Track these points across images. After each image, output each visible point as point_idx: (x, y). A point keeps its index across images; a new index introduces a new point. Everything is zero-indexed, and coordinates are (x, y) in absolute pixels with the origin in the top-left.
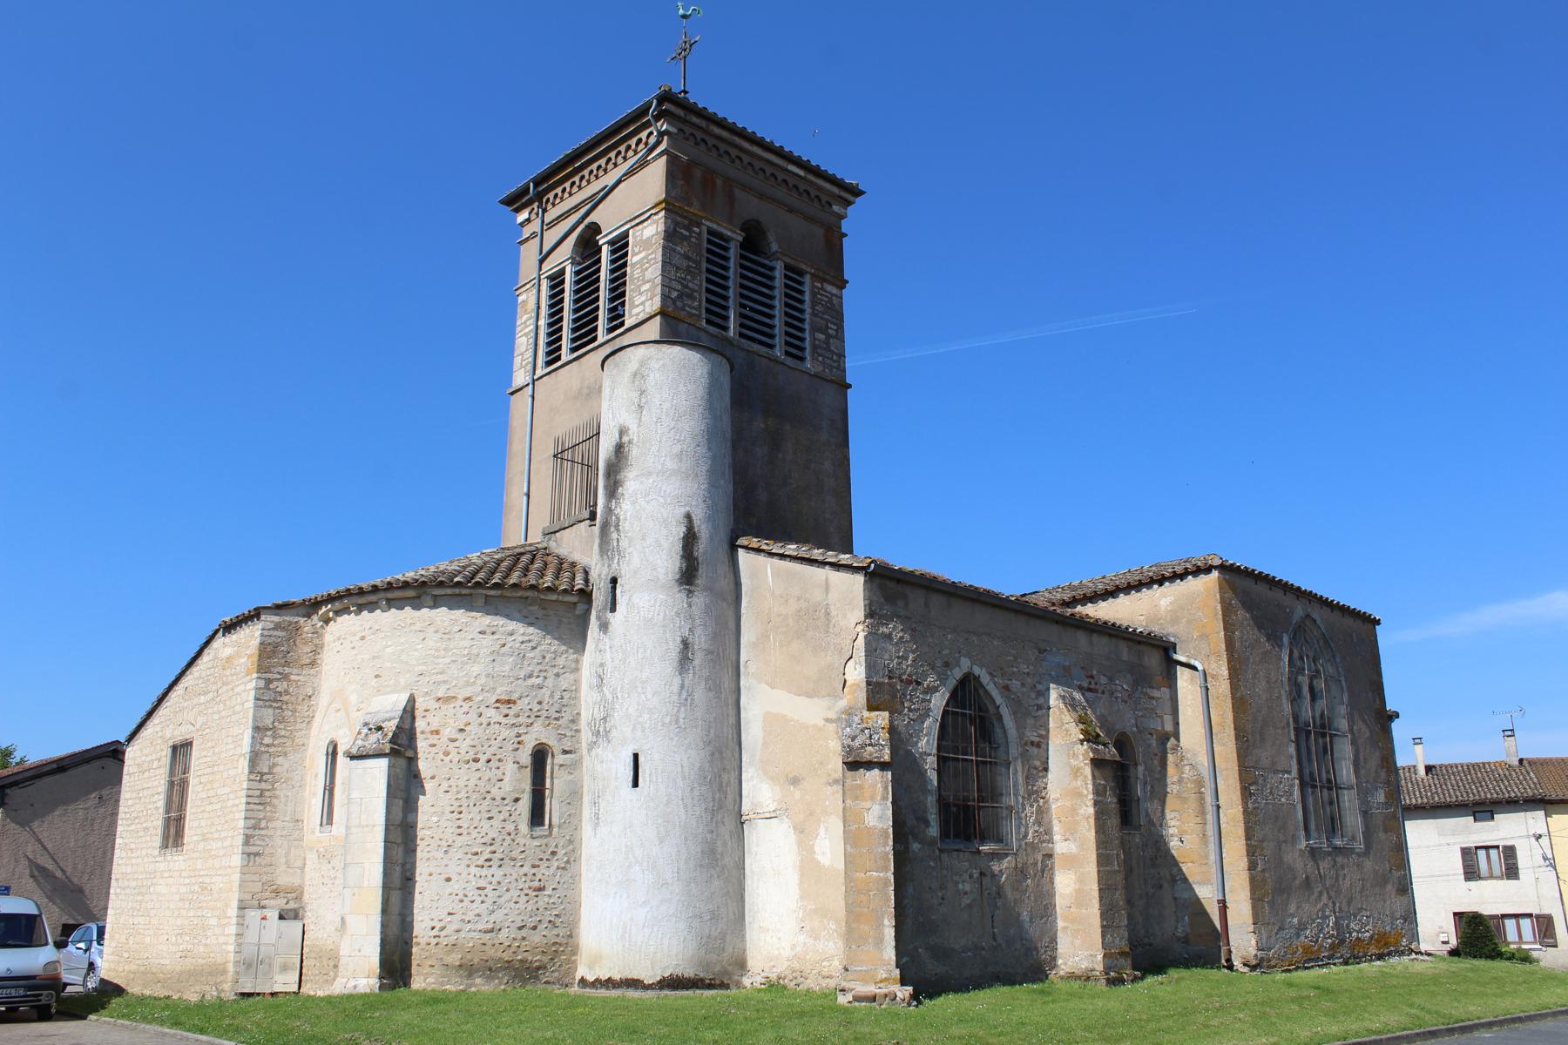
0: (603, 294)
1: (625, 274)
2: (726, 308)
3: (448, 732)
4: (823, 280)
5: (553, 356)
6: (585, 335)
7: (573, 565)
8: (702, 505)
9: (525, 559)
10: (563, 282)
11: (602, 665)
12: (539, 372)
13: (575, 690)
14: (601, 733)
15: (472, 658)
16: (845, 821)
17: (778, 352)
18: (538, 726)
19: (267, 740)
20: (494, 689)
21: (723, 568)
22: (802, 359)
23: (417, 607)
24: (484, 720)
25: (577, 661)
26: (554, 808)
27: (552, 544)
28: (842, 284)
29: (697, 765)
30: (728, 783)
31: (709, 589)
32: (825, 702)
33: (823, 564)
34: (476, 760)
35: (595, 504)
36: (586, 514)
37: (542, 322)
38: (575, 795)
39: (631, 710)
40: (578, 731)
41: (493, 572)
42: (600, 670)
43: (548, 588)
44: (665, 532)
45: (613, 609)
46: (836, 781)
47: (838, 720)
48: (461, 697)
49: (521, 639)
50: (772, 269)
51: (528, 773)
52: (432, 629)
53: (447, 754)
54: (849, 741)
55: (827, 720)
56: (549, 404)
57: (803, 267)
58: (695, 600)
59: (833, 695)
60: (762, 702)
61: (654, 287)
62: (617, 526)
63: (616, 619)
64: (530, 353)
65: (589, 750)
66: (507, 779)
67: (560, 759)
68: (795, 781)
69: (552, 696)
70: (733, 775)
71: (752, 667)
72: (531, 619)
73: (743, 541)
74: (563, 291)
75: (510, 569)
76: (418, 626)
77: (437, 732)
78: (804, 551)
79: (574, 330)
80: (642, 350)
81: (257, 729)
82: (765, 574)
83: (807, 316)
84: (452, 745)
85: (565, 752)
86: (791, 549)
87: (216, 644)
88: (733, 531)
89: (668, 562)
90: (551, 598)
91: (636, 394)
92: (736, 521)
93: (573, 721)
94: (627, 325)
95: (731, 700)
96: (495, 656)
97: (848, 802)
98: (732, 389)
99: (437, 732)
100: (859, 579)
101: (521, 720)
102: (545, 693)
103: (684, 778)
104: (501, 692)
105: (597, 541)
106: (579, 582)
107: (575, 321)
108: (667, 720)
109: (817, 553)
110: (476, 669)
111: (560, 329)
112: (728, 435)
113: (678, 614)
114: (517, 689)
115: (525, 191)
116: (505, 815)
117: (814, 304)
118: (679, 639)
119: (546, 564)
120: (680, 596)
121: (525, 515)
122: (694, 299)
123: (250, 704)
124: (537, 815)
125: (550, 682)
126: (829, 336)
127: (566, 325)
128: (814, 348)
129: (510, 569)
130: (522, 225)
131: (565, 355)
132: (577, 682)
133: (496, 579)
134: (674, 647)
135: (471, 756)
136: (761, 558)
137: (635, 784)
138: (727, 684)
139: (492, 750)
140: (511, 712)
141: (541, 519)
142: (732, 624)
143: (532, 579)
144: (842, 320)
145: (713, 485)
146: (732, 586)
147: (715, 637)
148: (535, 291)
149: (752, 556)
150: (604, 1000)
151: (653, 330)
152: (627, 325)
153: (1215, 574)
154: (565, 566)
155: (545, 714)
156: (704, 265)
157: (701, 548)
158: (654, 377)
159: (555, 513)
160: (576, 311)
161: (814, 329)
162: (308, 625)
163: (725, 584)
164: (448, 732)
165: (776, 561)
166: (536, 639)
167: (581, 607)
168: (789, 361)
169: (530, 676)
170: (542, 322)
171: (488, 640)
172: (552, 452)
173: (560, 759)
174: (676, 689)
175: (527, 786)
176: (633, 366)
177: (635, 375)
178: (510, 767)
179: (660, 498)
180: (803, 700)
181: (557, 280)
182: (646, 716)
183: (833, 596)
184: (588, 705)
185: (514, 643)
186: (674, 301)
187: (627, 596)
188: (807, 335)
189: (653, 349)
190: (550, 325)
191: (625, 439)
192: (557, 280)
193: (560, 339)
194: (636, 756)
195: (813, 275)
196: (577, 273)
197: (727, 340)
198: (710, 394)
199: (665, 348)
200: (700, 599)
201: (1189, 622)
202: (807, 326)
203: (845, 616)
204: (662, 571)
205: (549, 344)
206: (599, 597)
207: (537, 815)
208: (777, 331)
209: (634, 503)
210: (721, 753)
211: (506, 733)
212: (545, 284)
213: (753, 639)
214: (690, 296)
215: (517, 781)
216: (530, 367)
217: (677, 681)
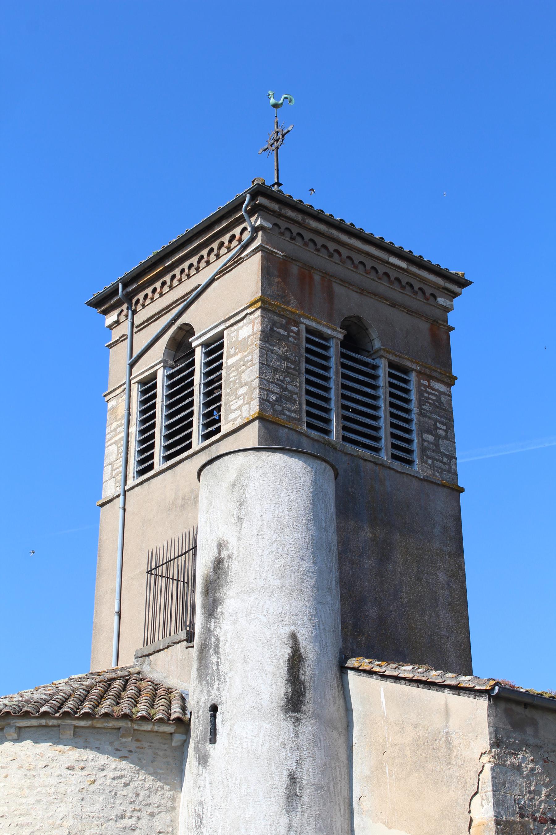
5: (145, 465)
45: (213, 740)
52: (15, 765)
61: (252, 390)
62: (217, 648)
91: (234, 506)
94: (224, 430)
100: (483, 703)
110: (63, 809)
115: (115, 292)
165: (389, 684)
183: (454, 723)
191: (224, 554)
209: (234, 622)
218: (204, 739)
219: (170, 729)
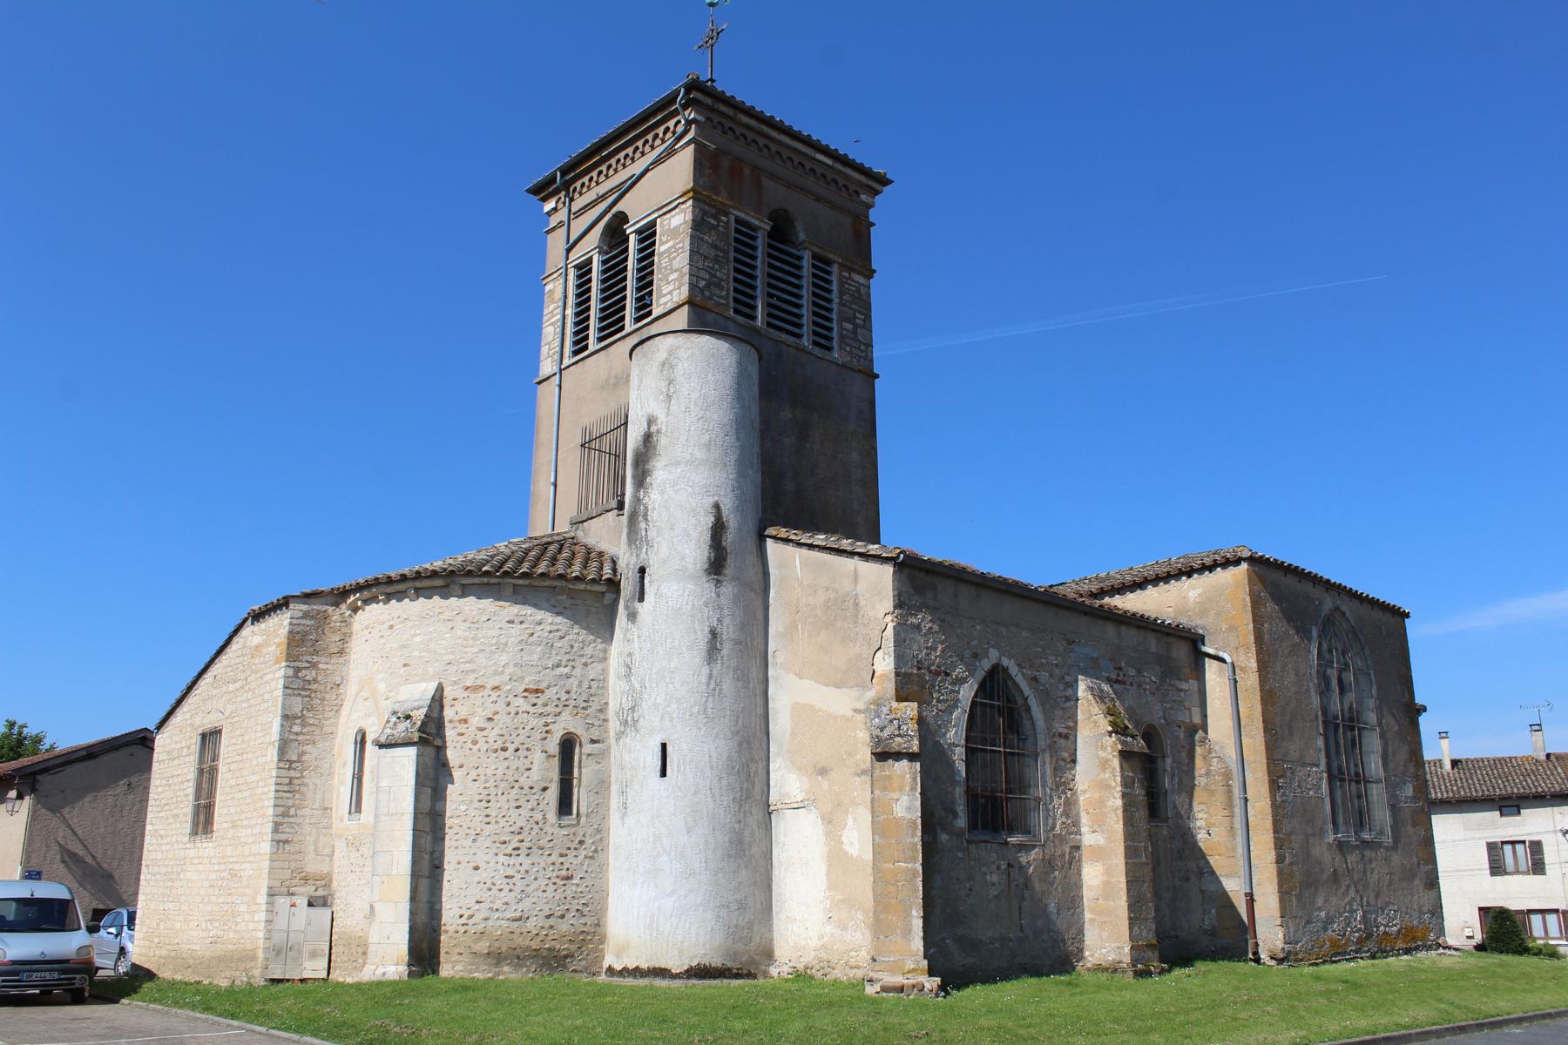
1: (652, 264)
2: (754, 298)
3: (476, 721)
4: (850, 270)
5: (580, 345)
6: (612, 325)
7: (601, 554)
8: (731, 495)
10: (590, 271)
11: (630, 655)
12: (566, 362)
13: (602, 681)
14: (630, 722)
15: (501, 647)
17: (805, 342)
19: (296, 729)
20: (522, 678)
21: (752, 558)
22: (829, 349)
23: (445, 597)
24: (512, 709)
25: (605, 651)
26: (582, 797)
27: (580, 534)
28: (870, 273)
29: (725, 755)
30: (756, 773)
31: (737, 579)
32: (854, 692)
33: (852, 554)
34: (504, 749)
35: (623, 495)
36: (614, 504)
37: (569, 312)
38: (602, 785)
40: (605, 720)
41: (521, 561)
44: (693, 521)
45: (641, 599)
46: (864, 772)
47: (867, 710)
48: (489, 686)
49: (549, 628)
50: (800, 258)
51: (556, 762)
52: (460, 618)
53: (475, 743)
54: (878, 732)
56: (577, 394)
57: (831, 256)
58: (723, 590)
59: (862, 686)
60: (790, 693)
62: (646, 515)
63: (644, 609)
64: (557, 342)
65: (617, 740)
66: (535, 768)
67: (588, 748)
68: (823, 772)
69: (580, 685)
70: (761, 765)
71: (780, 658)
72: (560, 609)
73: (771, 531)
74: (590, 280)
76: (446, 615)
77: (465, 721)
78: (832, 541)
79: (601, 320)
80: (670, 339)
81: (285, 717)
82: (794, 565)
83: (835, 306)
84: (481, 734)
85: (593, 741)
86: (820, 539)
87: (245, 632)
89: (695, 551)
90: (577, 587)
91: (663, 384)
92: (764, 511)
93: (601, 711)
97: (877, 792)
99: (465, 721)
100: (889, 570)
102: (574, 682)
103: (712, 768)
104: (529, 681)
105: (625, 531)
106: (607, 572)
107: (602, 310)
108: (695, 710)
109: (846, 544)
110: (504, 658)
111: (588, 318)
112: (757, 425)
113: (706, 604)
114: (547, 678)
115: (552, 179)
116: (533, 804)
117: (841, 293)
118: (707, 630)
119: (574, 554)
120: (708, 587)
121: (553, 503)
123: (279, 693)
124: (565, 804)
125: (578, 672)
126: (856, 326)
128: (842, 337)
130: (549, 214)
131: (593, 345)
132: (605, 671)
133: (525, 568)
135: (499, 745)
136: (790, 548)
137: (663, 773)
138: (755, 673)
140: (539, 702)
141: (568, 508)
142: (760, 615)
143: (560, 568)
145: (741, 474)
146: (760, 576)
147: (743, 627)
148: (562, 280)
149: (781, 546)
151: (681, 319)
153: (1244, 566)
155: (572, 703)
157: (729, 538)
158: (682, 367)
159: (583, 502)
160: (603, 300)
161: (842, 319)
162: (336, 614)
163: (753, 573)
164: (476, 721)
165: (804, 551)
166: (564, 629)
167: (609, 597)
168: (817, 351)
169: (558, 666)
170: (569, 312)
173: (588, 748)
174: (704, 679)
175: (555, 775)
176: (661, 355)
178: (538, 757)
179: (688, 488)
181: (584, 269)
182: (674, 706)
183: (861, 587)
184: (616, 695)
185: (542, 632)
186: (702, 290)
187: (654, 587)
188: (835, 325)
189: (681, 338)
191: (654, 428)
192: (584, 269)
194: (664, 746)
197: (755, 330)
198: (738, 383)
199: (694, 338)
200: (728, 589)
201: (1218, 614)
203: (873, 607)
205: (576, 333)
206: (627, 587)
207: (565, 804)
208: (804, 321)
209: (662, 492)
210: (749, 743)
211: (534, 722)
212: (572, 274)
215: (545, 769)
216: (557, 357)
217: (705, 670)
218: (633, 598)
219: (603, 589)
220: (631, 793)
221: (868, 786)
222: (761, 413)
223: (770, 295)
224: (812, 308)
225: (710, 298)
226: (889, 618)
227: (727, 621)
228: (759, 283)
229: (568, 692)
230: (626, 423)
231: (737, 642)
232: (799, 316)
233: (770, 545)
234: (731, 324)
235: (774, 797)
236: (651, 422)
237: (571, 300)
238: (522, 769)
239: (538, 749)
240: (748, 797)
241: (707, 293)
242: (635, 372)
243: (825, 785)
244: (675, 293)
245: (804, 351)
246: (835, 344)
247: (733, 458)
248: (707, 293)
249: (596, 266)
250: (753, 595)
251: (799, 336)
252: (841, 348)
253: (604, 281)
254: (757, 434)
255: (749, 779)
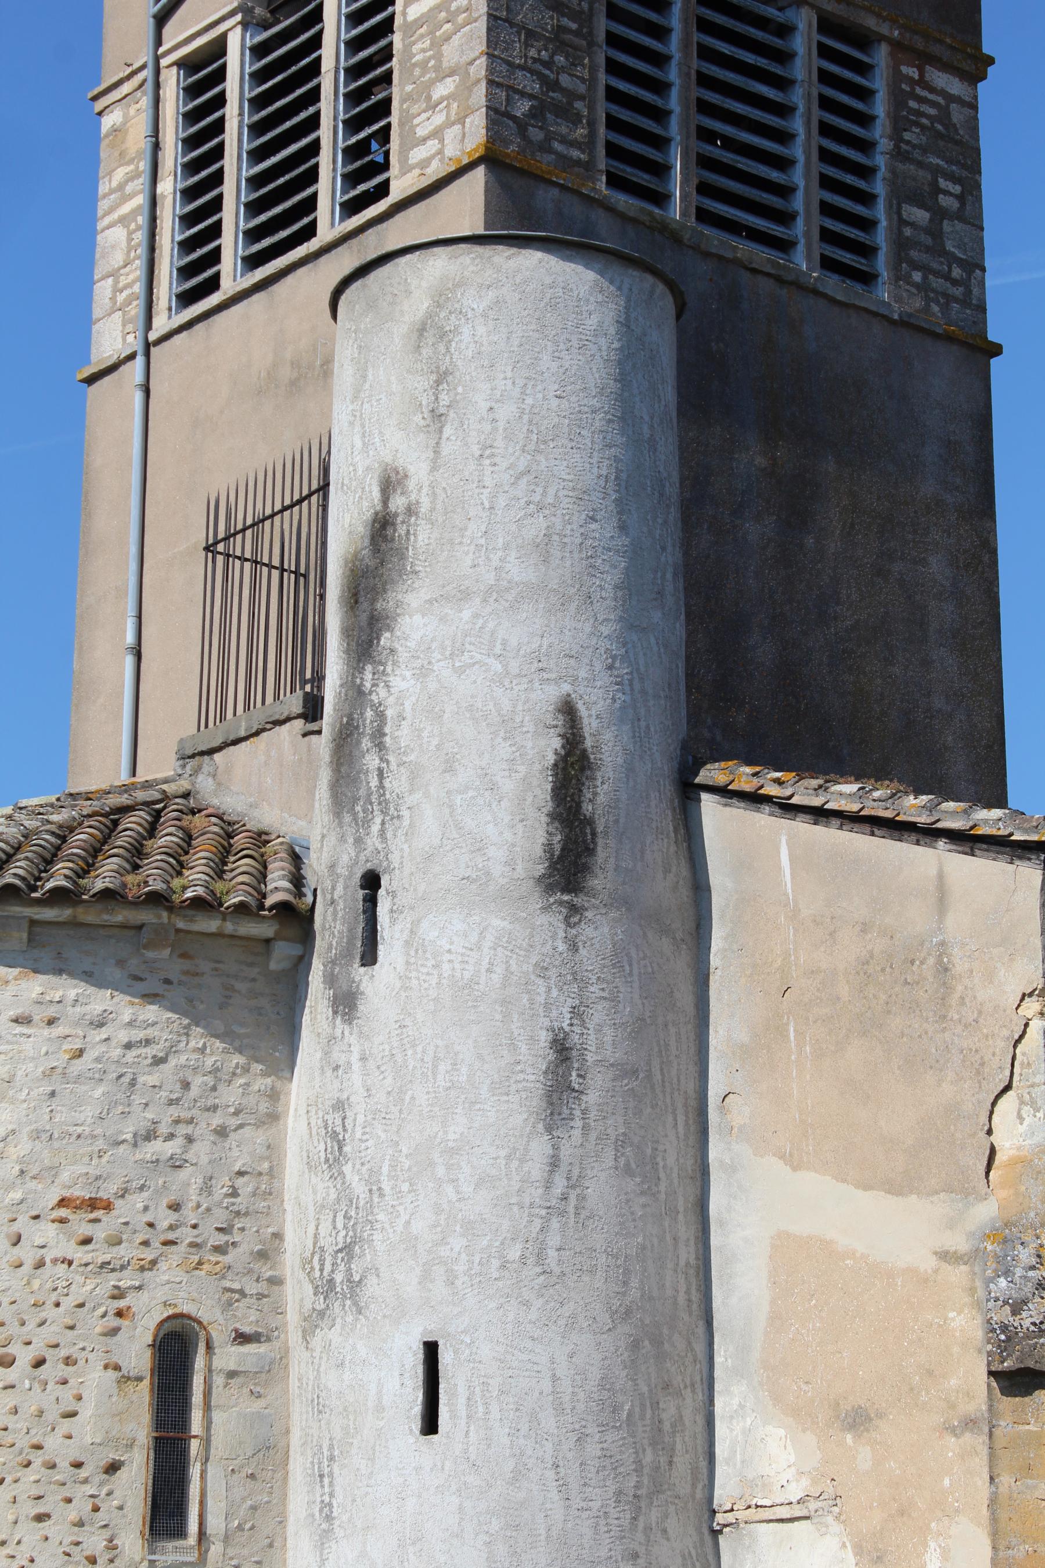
0: (331, 108)
1: (387, 54)
2: (661, 143)
4: (923, 59)
5: (198, 279)
6: (282, 222)
7: (261, 838)
8: (605, 679)
9: (133, 823)
10: (220, 75)
11: (340, 1106)
12: (162, 324)
13: (266, 1175)
14: (339, 1287)
16: (995, 1535)
17: (802, 261)
18: (170, 1270)
20: (54, 1170)
21: (662, 847)
22: (867, 278)
24: (26, 1253)
25: (274, 1095)
26: (213, 1490)
27: (204, 784)
28: (975, 66)
29: (595, 1374)
30: (678, 1421)
31: (623, 902)
33: (930, 834)
35: (319, 678)
36: (294, 703)
37: (166, 187)
38: (267, 1457)
39: (418, 1226)
40: (276, 1281)
41: (48, 860)
42: (334, 1119)
43: (197, 902)
44: (505, 750)
45: (369, 957)
46: (970, 1423)
47: (975, 1255)
49: (123, 1036)
50: (785, 30)
51: (143, 1395)
54: (1005, 1315)
55: (945, 1256)
56: (202, 407)
57: (871, 22)
58: (587, 931)
59: (961, 1190)
60: (767, 1207)
61: (466, 87)
62: (379, 734)
63: (377, 984)
64: (137, 271)
65: (307, 1334)
66: (87, 1411)
67: (229, 1356)
68: (858, 1421)
69: (207, 1188)
70: (691, 1402)
71: (740, 1111)
72: (153, 985)
73: (712, 773)
74: (220, 101)
75: (95, 852)
78: (878, 799)
79: (254, 208)
80: (439, 261)
82: (770, 860)
83: (881, 161)
85: (242, 1338)
86: (844, 794)
88: (685, 747)
89: (512, 830)
90: (210, 930)
91: (421, 384)
92: (694, 718)
93: (262, 1255)
94: (396, 193)
95: (684, 1201)
96: (56, 1083)
97: (1006, 1480)
98: (680, 362)
101: (125, 1252)
102: (190, 1180)
103: (559, 1409)
104: (72, 1179)
105: (325, 776)
106: (278, 886)
107: (255, 182)
108: (514, 1253)
109: (913, 806)
111: (216, 205)
112: (672, 490)
113: (542, 971)
114: (121, 1167)
116: (81, 1507)
117: (899, 125)
118: (544, 1037)
119: (189, 837)
120: (546, 924)
121: (127, 707)
122: (576, 120)
124: (167, 1508)
125: (202, 1151)
126: (940, 214)
127: (233, 193)
128: (901, 246)
129: (95, 852)
131: (232, 276)
132: (273, 1151)
133: (58, 878)
134: (533, 1058)
136: (763, 820)
137: (430, 1425)
138: (673, 1156)
139: (48, 1334)
140: (100, 1233)
141: (174, 715)
142: (685, 998)
143: (153, 877)
144: (975, 168)
145: (632, 624)
146: (685, 893)
147: (638, 1030)
148: (145, 101)
149: (739, 814)
150: (779, 868)
151: (466, 205)
152: (396, 193)
154: (239, 841)
155: (187, 1235)
156: (602, 25)
157: (602, 795)
158: (473, 337)
159: (212, 702)
160: (257, 155)
161: (901, 195)
163: (665, 888)
166: (163, 1036)
167: (283, 952)
168: (834, 285)
169: (150, 1136)
170: (166, 187)
171: (37, 1041)
172: (200, 538)
173: (229, 1356)
174: (537, 1169)
175: (140, 1428)
176: (416, 305)
177: (422, 330)
178: (94, 1380)
179: (491, 659)
180: (873, 1204)
181: (204, 70)
182: (457, 1243)
183: (957, 923)
184: (303, 1211)
185: (104, 1048)
186: (522, 127)
187: (404, 923)
188: (880, 212)
189: (468, 257)
190: (189, 194)
191: (398, 503)
192: (204, 70)
193: (216, 231)
194: (431, 1350)
195: (897, 46)
196: (259, 51)
197: (671, 235)
198: (623, 379)
199: (503, 257)
200: (599, 930)
202: (879, 188)
204: (497, 854)
205: (187, 246)
206: (333, 925)
207: (167, 1508)
208: (798, 203)
209: (423, 673)
210: (657, 1342)
211: (84, 1287)
212: (172, 82)
213: (743, 1036)
214: (565, 112)
215: (115, 1416)
216: (136, 309)
217: (540, 1147)
218: (346, 954)
219: (265, 929)
220: (342, 1479)
221: (980, 1464)
222: (686, 451)
223: (706, 135)
224: (818, 167)
225: (545, 147)
226: (1032, 1007)
227: (598, 1014)
228: (674, 102)
229: (175, 1207)
230: (324, 488)
231: (625, 1071)
232: (785, 191)
233: (711, 810)
234: (600, 218)
235: (723, 1493)
236: (390, 483)
237: (172, 155)
238: (52, 1414)
239: (97, 1361)
240: (657, 1489)
241: (536, 134)
242: (345, 354)
243: (865, 1457)
244: (451, 134)
245: (798, 285)
246: (882, 264)
247: (612, 578)
248: (536, 134)
249: (236, 62)
250: (666, 944)
251: (785, 246)
252: (899, 277)
253: (258, 102)
254: (674, 514)
255: (659, 1438)
